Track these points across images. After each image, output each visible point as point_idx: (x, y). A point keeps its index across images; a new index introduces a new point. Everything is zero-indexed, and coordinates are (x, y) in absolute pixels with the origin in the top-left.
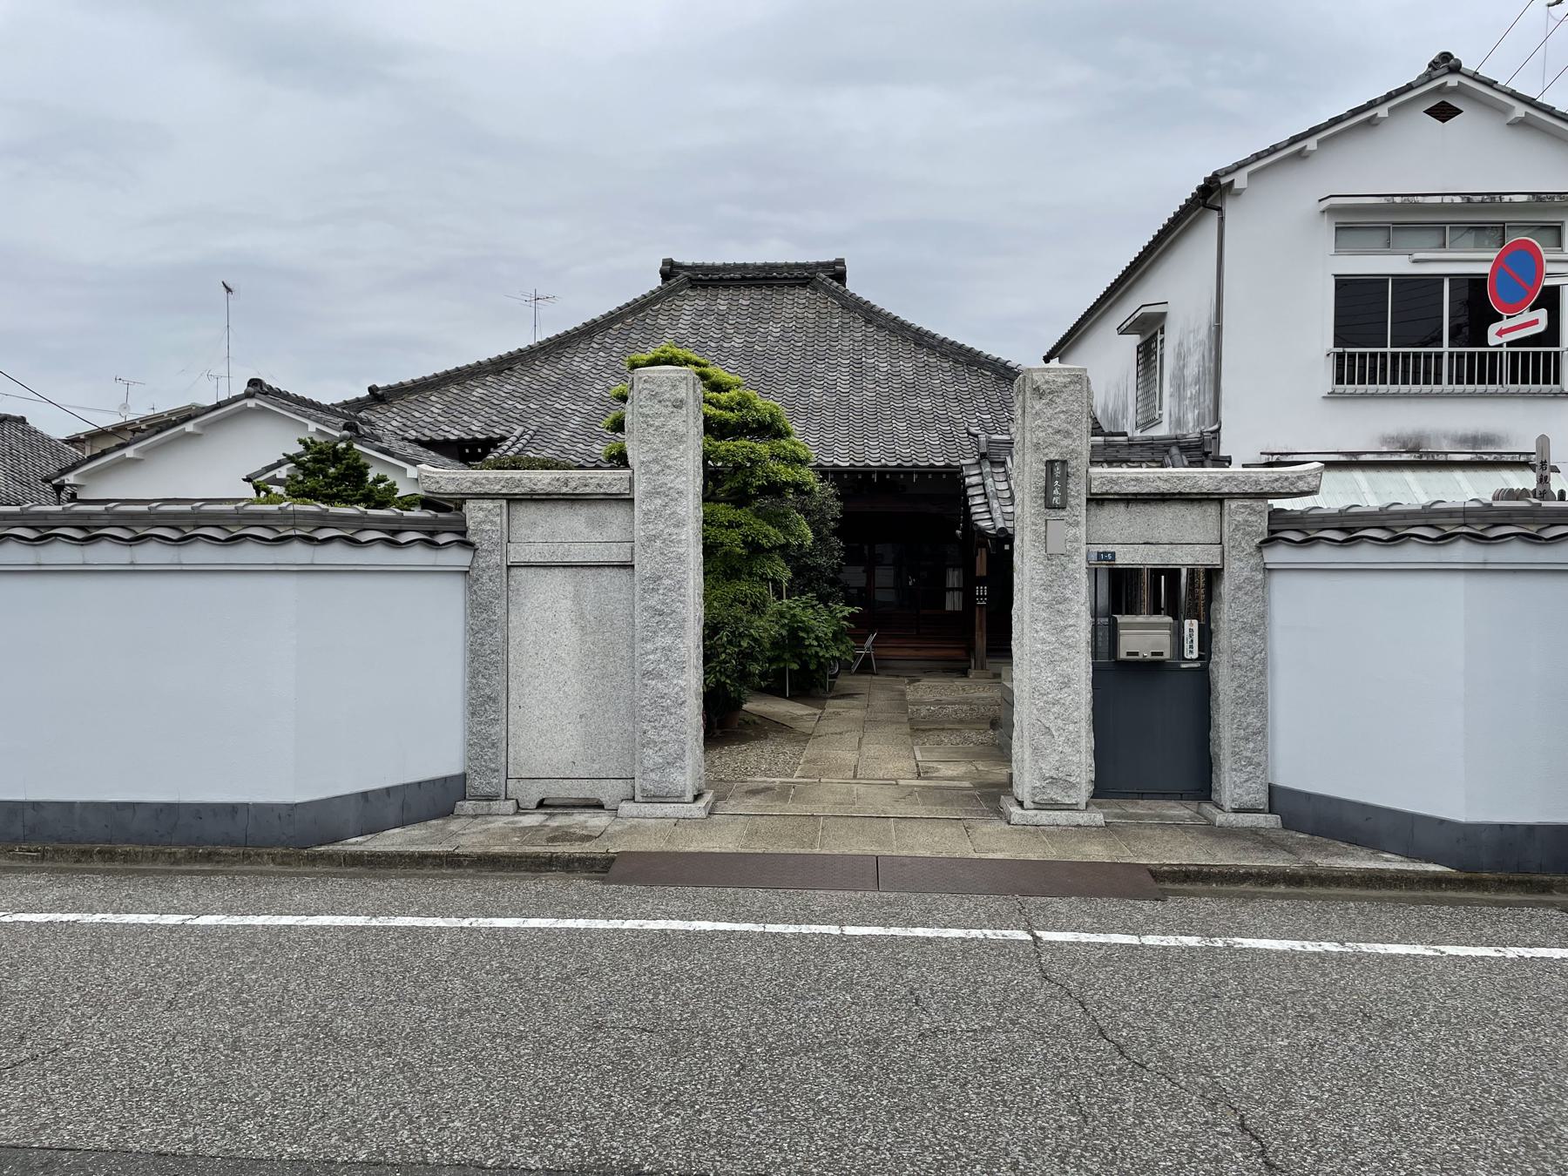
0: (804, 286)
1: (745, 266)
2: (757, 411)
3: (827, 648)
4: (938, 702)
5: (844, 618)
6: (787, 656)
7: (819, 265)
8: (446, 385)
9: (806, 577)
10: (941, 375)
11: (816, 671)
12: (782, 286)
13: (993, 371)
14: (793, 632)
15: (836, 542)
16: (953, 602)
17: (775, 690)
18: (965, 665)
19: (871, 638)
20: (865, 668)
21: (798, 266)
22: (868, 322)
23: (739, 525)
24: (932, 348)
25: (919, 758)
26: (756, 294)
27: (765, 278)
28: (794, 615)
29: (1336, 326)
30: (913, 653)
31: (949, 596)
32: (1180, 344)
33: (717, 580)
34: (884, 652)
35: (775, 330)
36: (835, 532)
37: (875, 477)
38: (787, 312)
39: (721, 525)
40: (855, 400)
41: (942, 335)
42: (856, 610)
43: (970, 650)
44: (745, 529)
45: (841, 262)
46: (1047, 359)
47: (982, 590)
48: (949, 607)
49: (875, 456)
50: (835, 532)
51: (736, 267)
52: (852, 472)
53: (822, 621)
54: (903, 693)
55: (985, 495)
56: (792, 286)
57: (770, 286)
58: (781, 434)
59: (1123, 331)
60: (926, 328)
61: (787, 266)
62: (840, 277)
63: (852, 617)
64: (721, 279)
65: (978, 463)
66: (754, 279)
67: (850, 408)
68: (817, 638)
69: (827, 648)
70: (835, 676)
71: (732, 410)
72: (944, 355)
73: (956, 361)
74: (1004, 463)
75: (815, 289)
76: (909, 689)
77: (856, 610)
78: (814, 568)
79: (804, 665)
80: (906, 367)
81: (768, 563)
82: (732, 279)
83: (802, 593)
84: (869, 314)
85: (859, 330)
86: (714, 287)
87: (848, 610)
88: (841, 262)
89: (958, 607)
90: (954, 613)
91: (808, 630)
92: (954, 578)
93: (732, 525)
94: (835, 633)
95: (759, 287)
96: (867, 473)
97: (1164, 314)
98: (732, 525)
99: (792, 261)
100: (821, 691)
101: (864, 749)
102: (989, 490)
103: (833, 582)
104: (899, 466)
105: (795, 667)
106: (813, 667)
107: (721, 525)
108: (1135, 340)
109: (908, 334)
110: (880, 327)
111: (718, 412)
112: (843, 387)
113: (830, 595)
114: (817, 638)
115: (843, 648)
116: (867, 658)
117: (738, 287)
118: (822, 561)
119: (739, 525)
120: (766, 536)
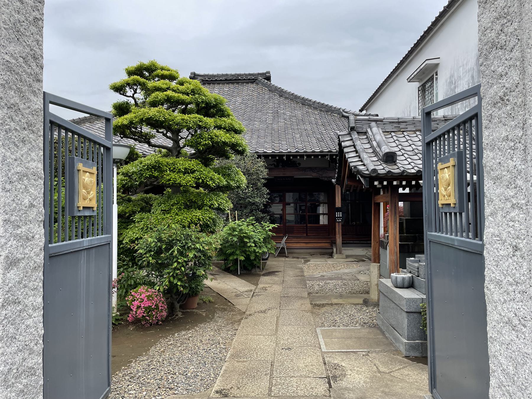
0: (252, 83)
1: (227, 75)
2: (205, 96)
4: (322, 278)
5: (270, 230)
6: (238, 252)
7: (259, 74)
8: (84, 123)
9: (243, 207)
10: (314, 116)
11: (255, 260)
12: (243, 83)
13: (338, 114)
14: (241, 239)
15: (266, 190)
16: (323, 220)
17: (230, 269)
18: (330, 251)
19: (285, 239)
20: (282, 253)
21: (250, 75)
22: (281, 96)
23: (193, 172)
24: (310, 105)
25: (324, 349)
26: (231, 86)
27: (235, 80)
28: (241, 230)
31: (321, 217)
32: (452, 76)
33: (180, 209)
34: (290, 245)
35: (239, 100)
36: (265, 185)
37: (285, 158)
38: (245, 93)
39: (179, 171)
40: (275, 126)
41: (314, 100)
42: (275, 226)
43: (333, 243)
44: (197, 174)
45: (269, 73)
46: (361, 111)
47: (339, 214)
49: (285, 147)
50: (265, 185)
51: (223, 75)
52: (273, 156)
53: (256, 231)
54: (302, 270)
55: (356, 151)
56: (247, 83)
57: (238, 83)
58: (222, 113)
59: (410, 80)
60: (306, 97)
61: (246, 75)
62: (268, 78)
63: (273, 230)
64: (216, 80)
65: (349, 134)
66: (231, 80)
67: (273, 129)
68: (255, 242)
70: (267, 259)
71: (188, 94)
72: (315, 108)
73: (321, 111)
74: (365, 133)
75: (257, 84)
76: (305, 267)
77: (275, 226)
78: (254, 204)
79: (248, 258)
80: (299, 113)
81: (214, 198)
82: (221, 80)
83: (247, 217)
84: (281, 93)
85: (277, 99)
86: (213, 84)
87: (272, 226)
88: (269, 73)
90: (324, 226)
91: (249, 237)
92: (322, 209)
93: (187, 171)
94: (264, 239)
95: (233, 83)
96: (281, 156)
97: (437, 65)
98: (187, 171)
99: (247, 73)
100: (258, 270)
101: (280, 333)
102: (358, 148)
103: (263, 211)
104: (297, 152)
105: (242, 258)
106: (252, 258)
107: (179, 171)
108: (416, 85)
109: (298, 100)
110: (286, 98)
111: (176, 95)
112: (269, 121)
114: (255, 242)
115: (269, 246)
116: (283, 248)
117: (223, 84)
118: (257, 200)
119: (193, 172)
120: (211, 179)
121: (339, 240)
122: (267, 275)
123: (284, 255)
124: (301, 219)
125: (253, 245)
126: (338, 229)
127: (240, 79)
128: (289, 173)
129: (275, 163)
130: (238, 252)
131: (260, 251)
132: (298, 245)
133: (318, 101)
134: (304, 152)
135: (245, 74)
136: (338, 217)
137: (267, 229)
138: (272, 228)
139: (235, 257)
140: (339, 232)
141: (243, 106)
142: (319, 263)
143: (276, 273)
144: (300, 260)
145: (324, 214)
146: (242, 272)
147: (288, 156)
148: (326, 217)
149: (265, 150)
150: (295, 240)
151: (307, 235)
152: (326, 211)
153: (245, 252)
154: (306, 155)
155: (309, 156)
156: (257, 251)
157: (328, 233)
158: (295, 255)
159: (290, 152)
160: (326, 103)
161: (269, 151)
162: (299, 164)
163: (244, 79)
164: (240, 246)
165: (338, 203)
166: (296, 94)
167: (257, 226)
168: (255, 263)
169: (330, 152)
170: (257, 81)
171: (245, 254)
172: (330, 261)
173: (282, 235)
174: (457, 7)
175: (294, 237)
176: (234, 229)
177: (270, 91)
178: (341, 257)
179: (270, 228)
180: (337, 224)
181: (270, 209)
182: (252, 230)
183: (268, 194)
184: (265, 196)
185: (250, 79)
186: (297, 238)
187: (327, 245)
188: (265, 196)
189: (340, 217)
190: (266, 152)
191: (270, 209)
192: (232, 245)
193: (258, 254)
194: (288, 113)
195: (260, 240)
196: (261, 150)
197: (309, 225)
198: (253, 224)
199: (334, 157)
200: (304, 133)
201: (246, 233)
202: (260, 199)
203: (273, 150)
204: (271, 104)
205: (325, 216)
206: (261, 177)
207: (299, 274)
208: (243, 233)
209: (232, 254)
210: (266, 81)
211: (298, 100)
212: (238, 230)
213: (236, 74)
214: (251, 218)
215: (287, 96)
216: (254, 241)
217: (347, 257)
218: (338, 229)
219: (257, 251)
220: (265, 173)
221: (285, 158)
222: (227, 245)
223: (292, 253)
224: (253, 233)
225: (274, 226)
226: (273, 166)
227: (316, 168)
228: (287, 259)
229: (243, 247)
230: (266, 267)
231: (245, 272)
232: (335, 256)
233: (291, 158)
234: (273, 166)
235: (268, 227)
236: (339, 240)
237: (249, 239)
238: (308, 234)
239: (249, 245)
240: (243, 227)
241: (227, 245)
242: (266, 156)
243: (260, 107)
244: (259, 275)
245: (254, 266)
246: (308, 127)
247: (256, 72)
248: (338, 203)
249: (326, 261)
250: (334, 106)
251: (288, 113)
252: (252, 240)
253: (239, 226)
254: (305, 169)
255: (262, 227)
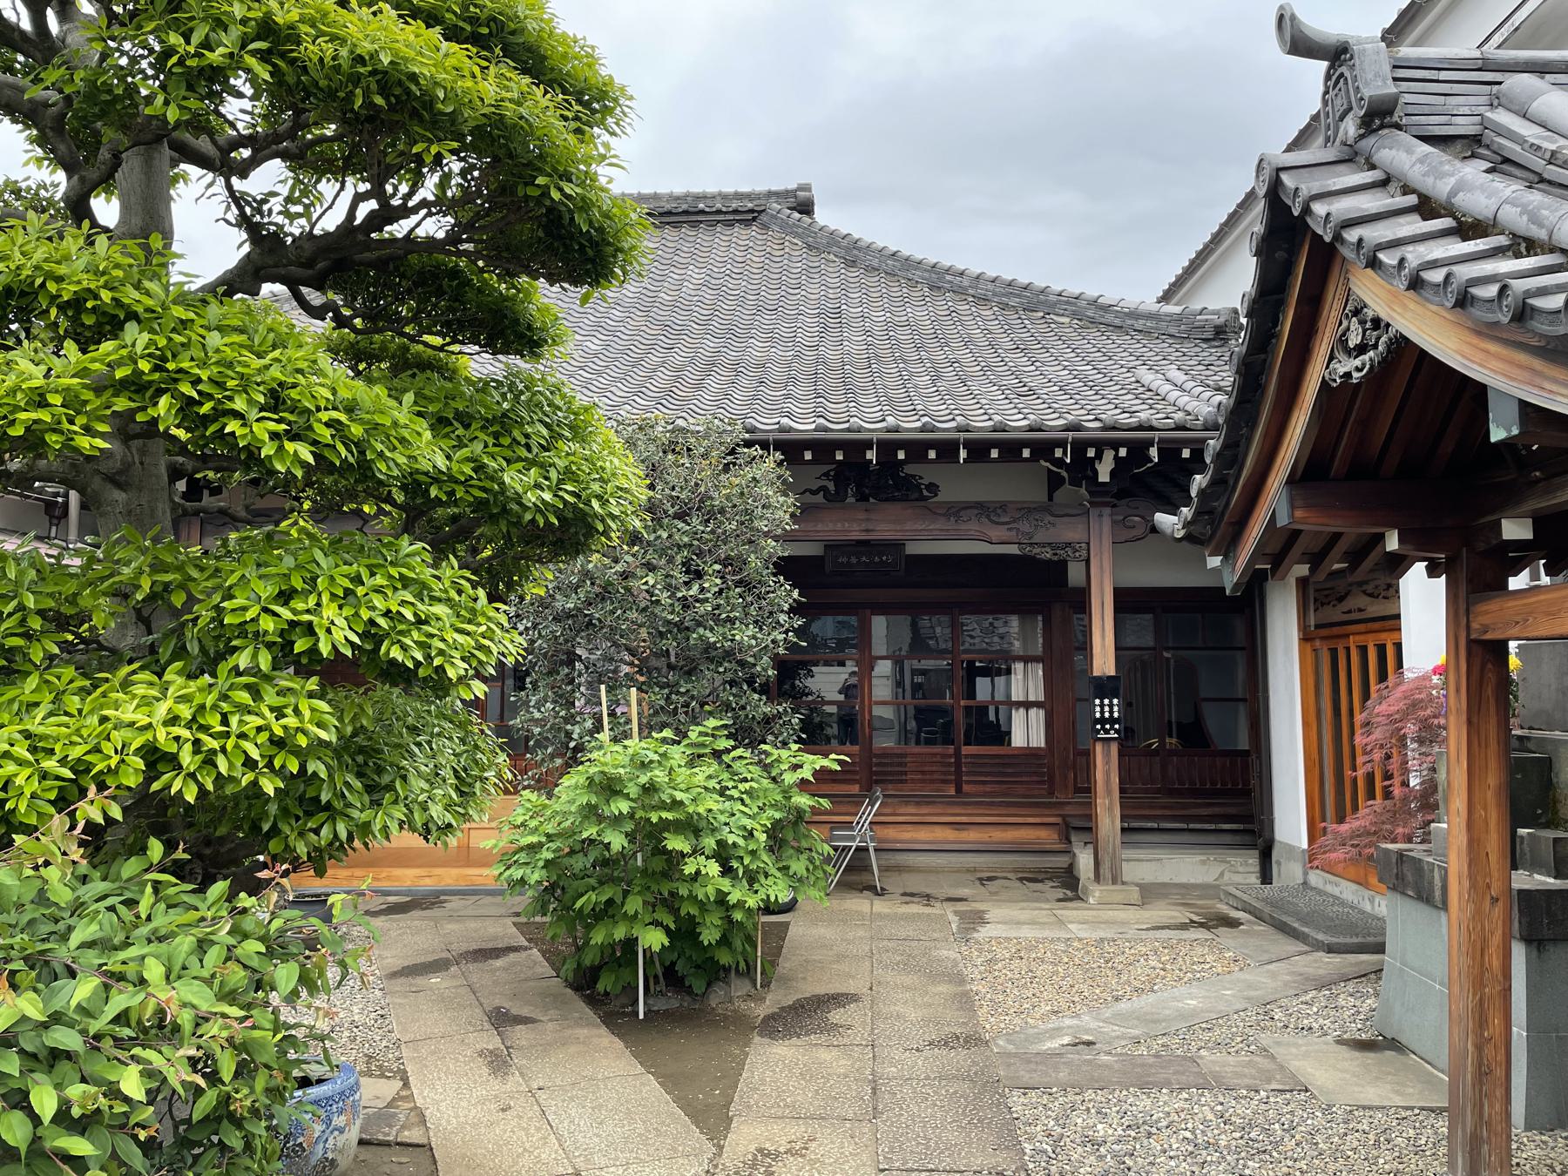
0: (747, 223)
3: (751, 877)
5: (803, 784)
6: (634, 905)
7: (770, 194)
9: (678, 676)
10: (980, 322)
14: (648, 835)
15: (786, 594)
16: (1027, 731)
18: (1061, 861)
20: (856, 875)
21: (738, 196)
22: (851, 264)
24: (959, 291)
27: (686, 212)
28: (650, 789)
29: (1423, 354)
30: (949, 834)
34: (890, 833)
35: (695, 275)
37: (871, 455)
40: (831, 354)
42: (830, 762)
43: (1081, 826)
48: (1018, 740)
52: (822, 447)
53: (726, 790)
56: (729, 224)
57: (694, 225)
61: (724, 197)
62: (806, 208)
68: (723, 855)
69: (751, 877)
72: (982, 300)
75: (765, 227)
78: (728, 654)
79: (685, 933)
80: (920, 314)
84: (852, 253)
85: (834, 271)
87: (813, 763)
89: (1038, 740)
90: (1029, 753)
91: (692, 827)
94: (774, 831)
106: (709, 936)
109: (917, 275)
110: (871, 269)
113: (767, 720)
115: (799, 866)
118: (745, 635)
121: (1108, 817)
122: (789, 1033)
123: (865, 877)
124: (929, 722)
125: (713, 868)
126: (1106, 767)
127: (702, 212)
128: (885, 524)
129: (831, 486)
130: (634, 905)
131: (752, 902)
132: (923, 835)
133: (992, 274)
134: (959, 429)
135: (720, 194)
136: (1102, 721)
137: (790, 778)
138: (816, 773)
139: (620, 933)
140: (1108, 781)
141: (708, 295)
142: (1027, 933)
143: (836, 1016)
144: (936, 909)
145: (1027, 705)
146: (660, 1005)
147: (887, 448)
148: (1037, 717)
149: (785, 421)
150: (909, 812)
151: (959, 790)
152: (1037, 693)
153: (671, 903)
154: (968, 444)
155: (979, 450)
156: (733, 898)
157: (1053, 783)
158: (914, 883)
159: (896, 430)
160: (1023, 280)
161: (805, 426)
162: (933, 488)
163: (719, 212)
164: (644, 872)
165: (1104, 661)
166: (906, 252)
167: (737, 766)
168: (724, 958)
169: (1076, 427)
170: (764, 218)
171: (675, 911)
172: (1070, 912)
173: (855, 789)
174: (1213, 265)
175: (906, 799)
176: (609, 787)
177: (809, 247)
178: (1119, 897)
179: (806, 773)
180: (1099, 747)
181: (809, 682)
182: (712, 784)
183: (795, 610)
184: (783, 618)
185: (744, 213)
186: (921, 801)
187: (1047, 837)
188: (783, 618)
189: (1112, 721)
190: (790, 430)
191: (809, 682)
192: (608, 866)
193: (738, 916)
194: (879, 316)
195: (750, 834)
196: (766, 423)
197: (966, 750)
198: (717, 754)
199: (1091, 453)
200: (949, 373)
201: (676, 804)
202: (763, 633)
203: (821, 420)
204: (814, 288)
205: (1033, 712)
206: (762, 525)
207: (954, 1023)
208: (663, 806)
209: (607, 912)
210: (797, 215)
211: (917, 275)
212: (633, 790)
213: (687, 195)
214: (712, 723)
215: (875, 263)
216: (721, 844)
217: (1150, 893)
218: (1106, 767)
219: (733, 898)
220: (779, 509)
221: (871, 455)
222: (579, 863)
223: (899, 869)
224: (712, 803)
225: (821, 762)
226: (820, 498)
227: (1003, 506)
228: (880, 906)
229: (666, 875)
230: (785, 965)
231: (674, 1004)
232: (1096, 893)
233: (901, 455)
234: (820, 498)
235: (796, 767)
236: (1108, 817)
237: (697, 832)
238: (966, 788)
239: (689, 869)
240: (660, 775)
241: (579, 863)
242: (790, 449)
243: (770, 297)
244: (741, 1027)
245: (715, 973)
246: (965, 356)
247: (761, 187)
248: (1104, 661)
249: (1061, 923)
250: (1057, 288)
251: (879, 316)
252: (709, 843)
253: (644, 766)
254: (956, 511)
255: (767, 768)
